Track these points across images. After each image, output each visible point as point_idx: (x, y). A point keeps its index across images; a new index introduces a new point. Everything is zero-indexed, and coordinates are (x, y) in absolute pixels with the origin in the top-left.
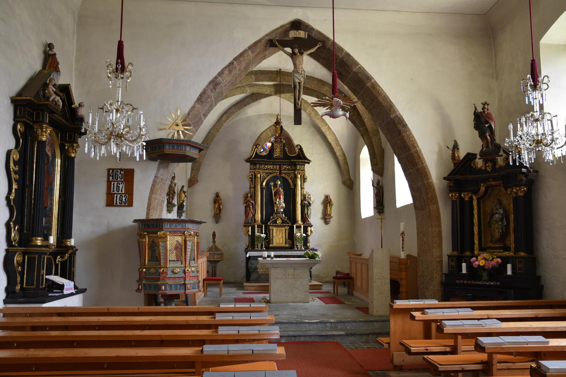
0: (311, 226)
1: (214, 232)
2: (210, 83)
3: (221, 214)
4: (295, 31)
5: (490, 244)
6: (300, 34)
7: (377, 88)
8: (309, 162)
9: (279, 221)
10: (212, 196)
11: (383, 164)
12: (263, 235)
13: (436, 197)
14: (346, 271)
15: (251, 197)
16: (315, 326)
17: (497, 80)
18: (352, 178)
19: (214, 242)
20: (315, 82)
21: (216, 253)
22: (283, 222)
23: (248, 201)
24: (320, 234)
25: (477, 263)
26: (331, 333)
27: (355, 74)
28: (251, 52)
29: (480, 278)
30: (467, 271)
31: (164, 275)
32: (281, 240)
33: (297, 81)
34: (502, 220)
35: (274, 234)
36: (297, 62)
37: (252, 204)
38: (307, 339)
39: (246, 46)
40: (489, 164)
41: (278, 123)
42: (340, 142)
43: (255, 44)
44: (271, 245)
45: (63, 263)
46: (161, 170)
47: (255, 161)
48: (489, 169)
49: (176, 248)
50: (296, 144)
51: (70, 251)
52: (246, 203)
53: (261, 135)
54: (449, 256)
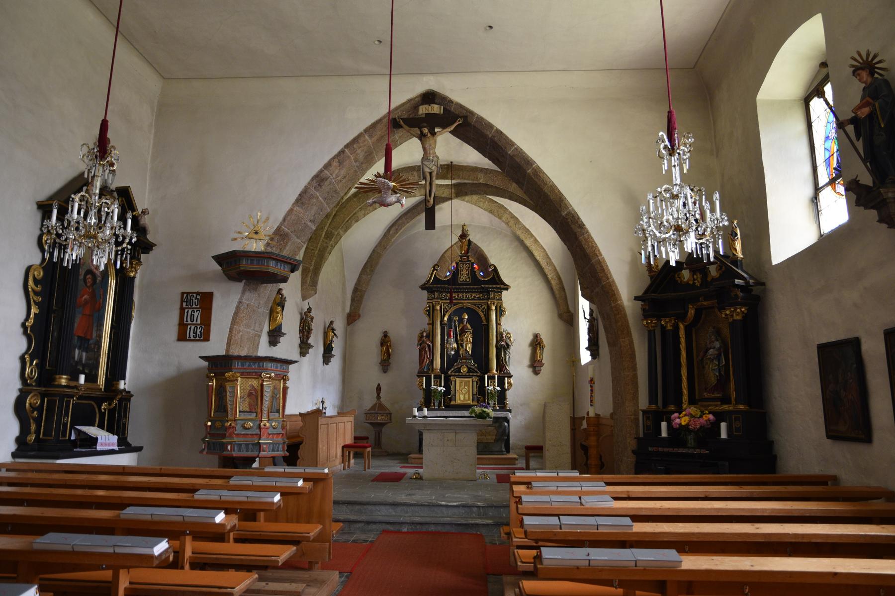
0: (511, 377)
1: (379, 385)
2: (313, 179)
3: (391, 361)
4: (426, 106)
5: (706, 395)
6: (433, 109)
7: (541, 175)
8: (507, 288)
9: (464, 370)
10: (378, 336)
13: (628, 327)
15: (428, 336)
16: (456, 510)
17: (717, 156)
18: (571, 309)
19: (379, 397)
21: (381, 412)
25: (678, 421)
26: (473, 522)
27: (511, 157)
29: (684, 444)
30: (669, 434)
31: (231, 430)
32: (467, 397)
33: (427, 170)
34: (718, 357)
36: (427, 146)
37: (429, 346)
38: (439, 528)
40: (698, 276)
41: (463, 236)
42: (553, 261)
43: (374, 126)
44: (452, 403)
45: (112, 412)
46: (247, 294)
47: (433, 287)
48: (698, 284)
49: (250, 395)
51: (119, 396)
54: (644, 412)
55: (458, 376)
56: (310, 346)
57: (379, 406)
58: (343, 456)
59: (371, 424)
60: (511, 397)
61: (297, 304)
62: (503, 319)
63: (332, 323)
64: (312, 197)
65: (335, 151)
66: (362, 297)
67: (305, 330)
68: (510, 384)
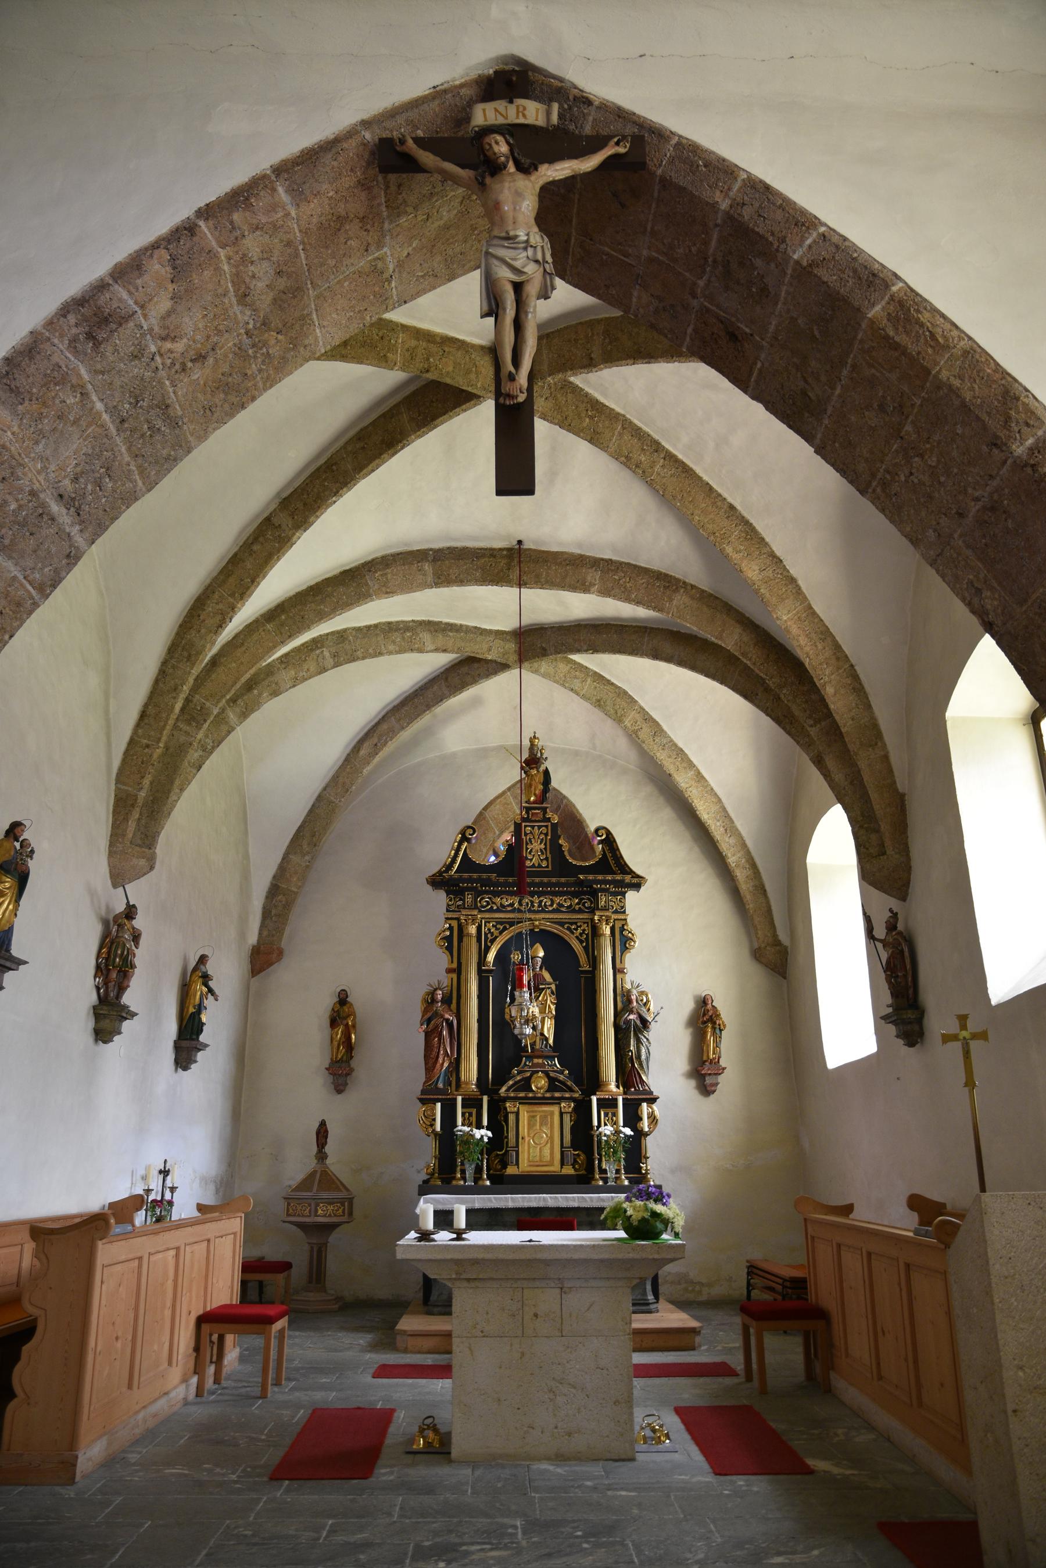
0: (652, 1100)
1: (323, 1124)
2: (65, 310)
3: (354, 1063)
4: (501, 105)
6: (521, 111)
7: (925, 317)
9: (540, 1083)
10: (326, 1002)
11: (905, 850)
12: (483, 1134)
14: (785, 1263)
15: (447, 1000)
18: (783, 937)
19: (321, 1155)
20: (642, 581)
21: (325, 1195)
22: (554, 1084)
23: (436, 1014)
24: (686, 1131)
27: (805, 273)
28: (289, 191)
32: (547, 1151)
33: (504, 274)
35: (524, 1130)
37: (450, 1025)
39: (263, 162)
42: (738, 824)
43: (310, 157)
44: (511, 1170)
47: (460, 881)
50: (592, 827)
52: (429, 1021)
53: (485, 808)
55: (524, 1101)
56: (125, 1014)
57: (321, 1179)
58: (197, 1349)
59: (301, 1226)
60: (660, 1159)
61: (92, 893)
62: (628, 957)
63: (203, 959)
64: (59, 377)
65: (163, 225)
66: (288, 906)
67: (114, 965)
68: (653, 1119)
